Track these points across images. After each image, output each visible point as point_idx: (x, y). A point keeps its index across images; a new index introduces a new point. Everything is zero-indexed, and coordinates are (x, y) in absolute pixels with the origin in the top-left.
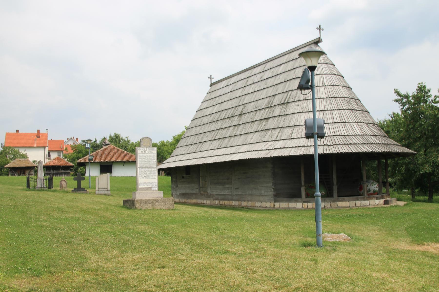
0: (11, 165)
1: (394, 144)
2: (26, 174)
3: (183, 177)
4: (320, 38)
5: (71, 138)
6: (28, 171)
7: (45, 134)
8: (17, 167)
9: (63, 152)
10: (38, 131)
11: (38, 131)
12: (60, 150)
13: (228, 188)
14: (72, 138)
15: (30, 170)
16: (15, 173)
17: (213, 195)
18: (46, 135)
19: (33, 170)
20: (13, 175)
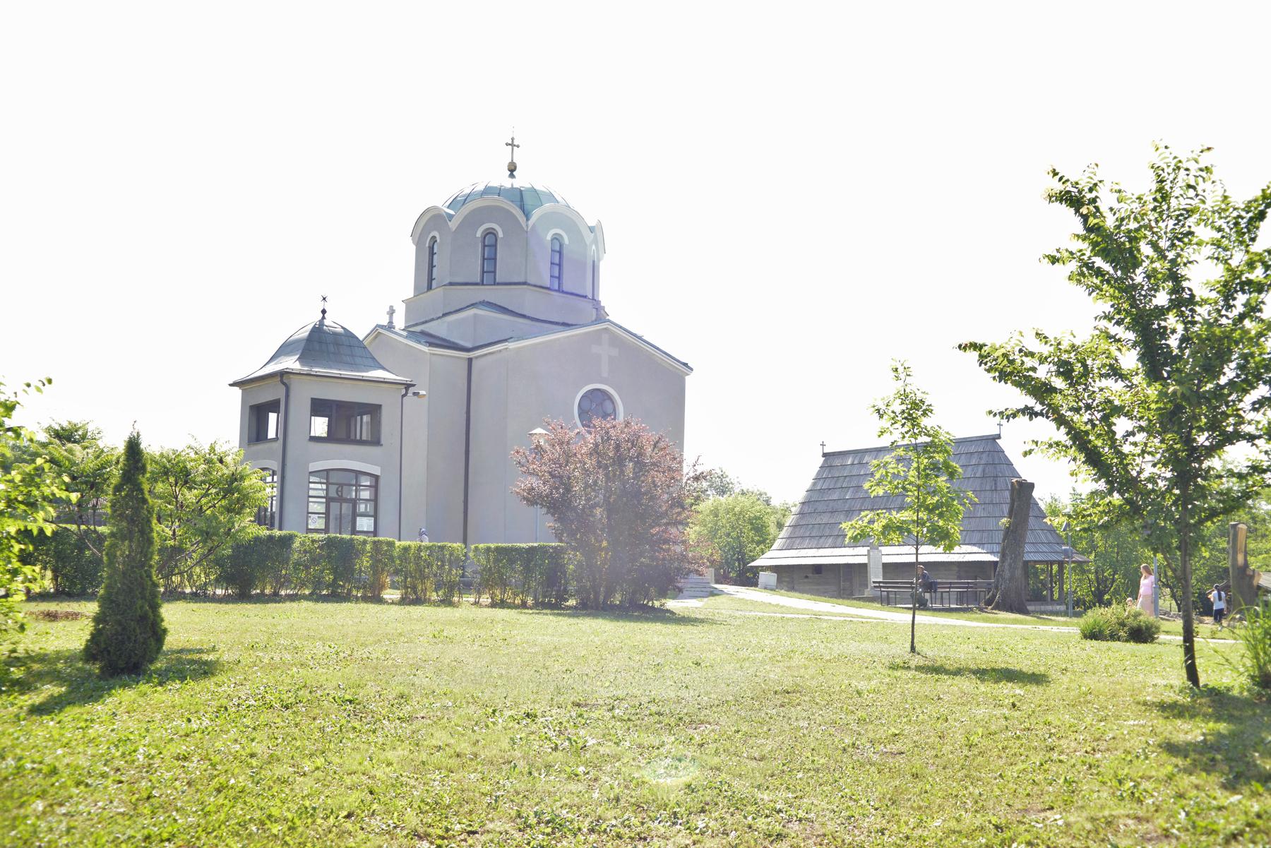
3: (807, 577)
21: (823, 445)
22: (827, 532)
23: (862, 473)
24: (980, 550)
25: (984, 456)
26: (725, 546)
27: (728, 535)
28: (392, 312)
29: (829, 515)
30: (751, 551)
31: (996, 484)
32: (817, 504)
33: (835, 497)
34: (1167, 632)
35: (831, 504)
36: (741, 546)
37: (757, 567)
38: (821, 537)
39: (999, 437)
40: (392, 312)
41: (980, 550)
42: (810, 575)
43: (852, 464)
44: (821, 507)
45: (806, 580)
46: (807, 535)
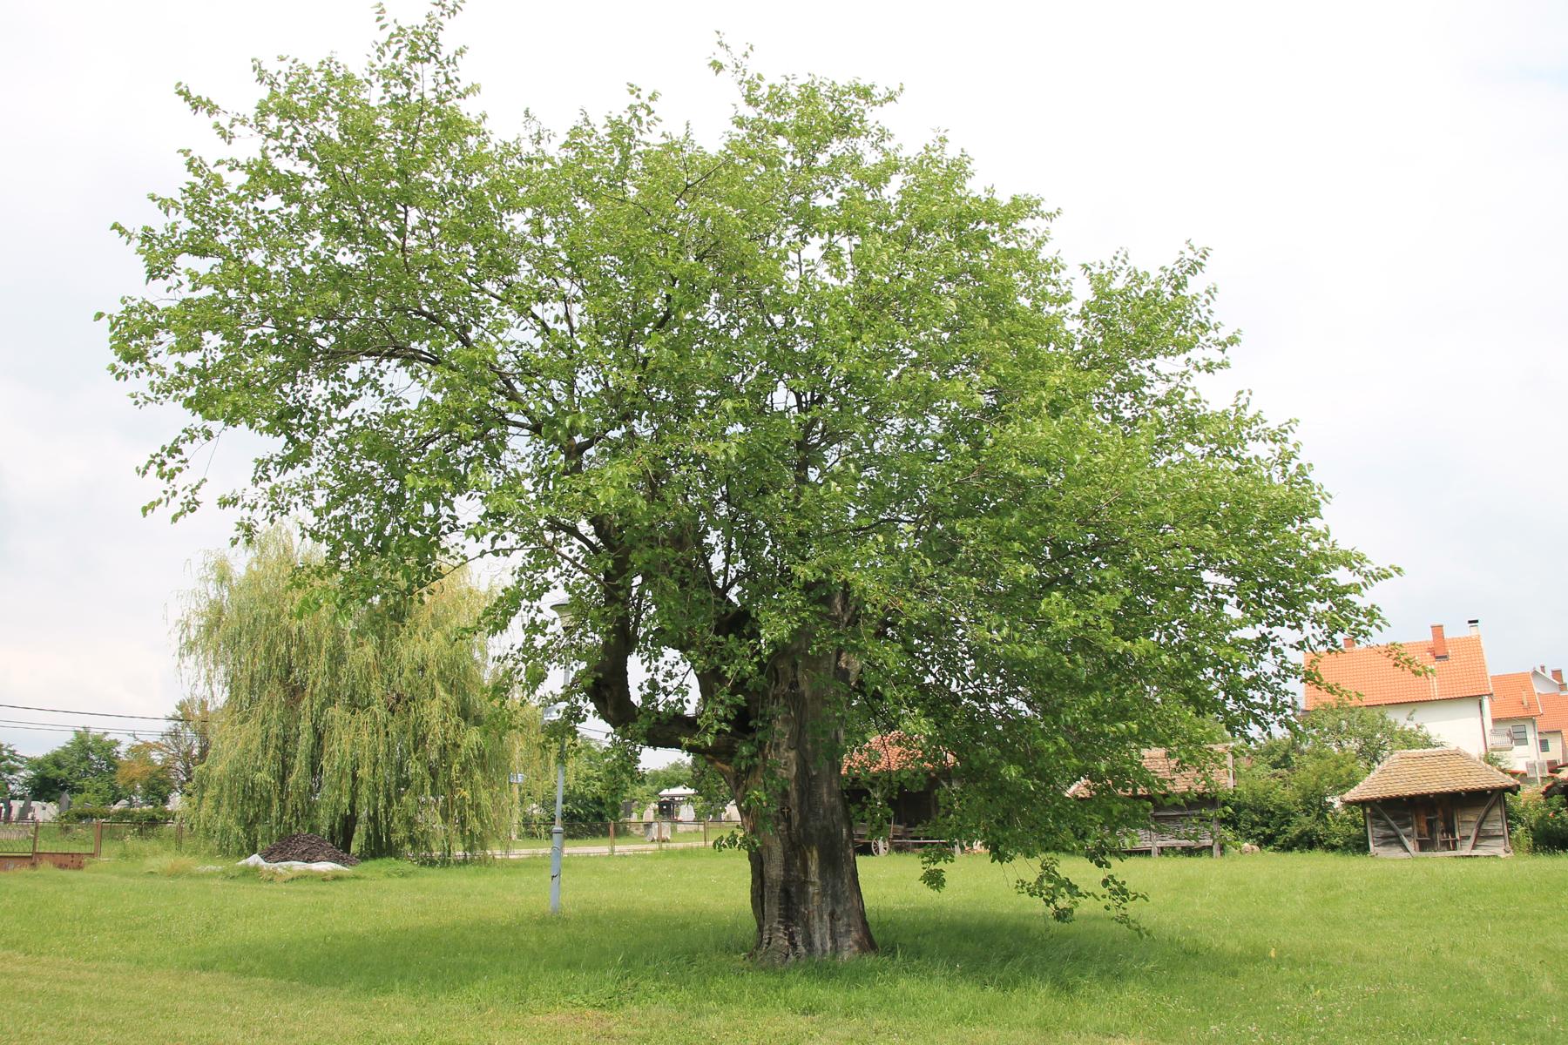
0: (1371, 786)
1: (1500, 750)
2: (1465, 832)
5: (1535, 673)
6: (1472, 817)
7: (1467, 640)
8: (1411, 798)
9: (1534, 723)
10: (1438, 630)
11: (1438, 630)
12: (1522, 714)
14: (1539, 670)
15: (1482, 812)
16: (1402, 832)
18: (1473, 646)
19: (1497, 812)
20: (1393, 840)
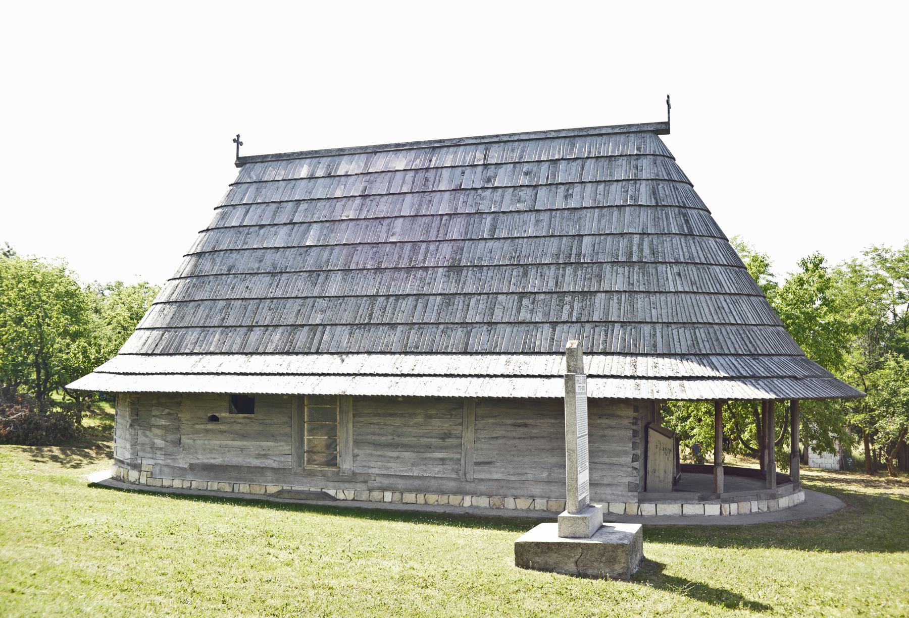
3: (214, 419)
4: (668, 124)
13: (442, 460)
17: (369, 475)
21: (237, 141)
22: (266, 317)
23: (338, 194)
24: (708, 372)
25: (645, 162)
26: (13, 340)
27: (19, 321)
28: (772, 275)
29: (268, 279)
30: (60, 351)
31: (687, 221)
32: (234, 255)
33: (280, 238)
34: (592, 346)
35: (269, 256)
36: (42, 339)
37: (89, 394)
38: (251, 328)
39: (664, 128)
40: (772, 275)
41: (708, 372)
42: (223, 415)
43: (311, 178)
44: (244, 263)
45: (211, 426)
46: (215, 321)
